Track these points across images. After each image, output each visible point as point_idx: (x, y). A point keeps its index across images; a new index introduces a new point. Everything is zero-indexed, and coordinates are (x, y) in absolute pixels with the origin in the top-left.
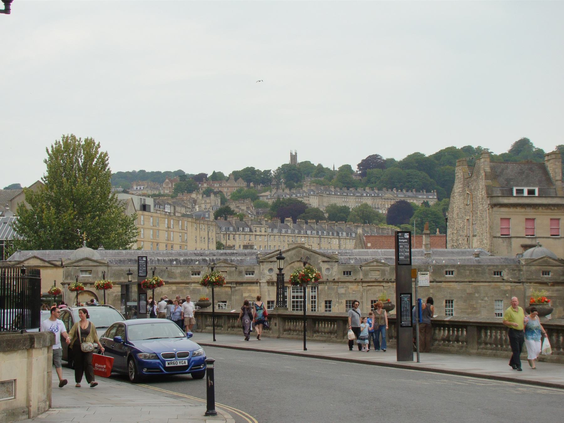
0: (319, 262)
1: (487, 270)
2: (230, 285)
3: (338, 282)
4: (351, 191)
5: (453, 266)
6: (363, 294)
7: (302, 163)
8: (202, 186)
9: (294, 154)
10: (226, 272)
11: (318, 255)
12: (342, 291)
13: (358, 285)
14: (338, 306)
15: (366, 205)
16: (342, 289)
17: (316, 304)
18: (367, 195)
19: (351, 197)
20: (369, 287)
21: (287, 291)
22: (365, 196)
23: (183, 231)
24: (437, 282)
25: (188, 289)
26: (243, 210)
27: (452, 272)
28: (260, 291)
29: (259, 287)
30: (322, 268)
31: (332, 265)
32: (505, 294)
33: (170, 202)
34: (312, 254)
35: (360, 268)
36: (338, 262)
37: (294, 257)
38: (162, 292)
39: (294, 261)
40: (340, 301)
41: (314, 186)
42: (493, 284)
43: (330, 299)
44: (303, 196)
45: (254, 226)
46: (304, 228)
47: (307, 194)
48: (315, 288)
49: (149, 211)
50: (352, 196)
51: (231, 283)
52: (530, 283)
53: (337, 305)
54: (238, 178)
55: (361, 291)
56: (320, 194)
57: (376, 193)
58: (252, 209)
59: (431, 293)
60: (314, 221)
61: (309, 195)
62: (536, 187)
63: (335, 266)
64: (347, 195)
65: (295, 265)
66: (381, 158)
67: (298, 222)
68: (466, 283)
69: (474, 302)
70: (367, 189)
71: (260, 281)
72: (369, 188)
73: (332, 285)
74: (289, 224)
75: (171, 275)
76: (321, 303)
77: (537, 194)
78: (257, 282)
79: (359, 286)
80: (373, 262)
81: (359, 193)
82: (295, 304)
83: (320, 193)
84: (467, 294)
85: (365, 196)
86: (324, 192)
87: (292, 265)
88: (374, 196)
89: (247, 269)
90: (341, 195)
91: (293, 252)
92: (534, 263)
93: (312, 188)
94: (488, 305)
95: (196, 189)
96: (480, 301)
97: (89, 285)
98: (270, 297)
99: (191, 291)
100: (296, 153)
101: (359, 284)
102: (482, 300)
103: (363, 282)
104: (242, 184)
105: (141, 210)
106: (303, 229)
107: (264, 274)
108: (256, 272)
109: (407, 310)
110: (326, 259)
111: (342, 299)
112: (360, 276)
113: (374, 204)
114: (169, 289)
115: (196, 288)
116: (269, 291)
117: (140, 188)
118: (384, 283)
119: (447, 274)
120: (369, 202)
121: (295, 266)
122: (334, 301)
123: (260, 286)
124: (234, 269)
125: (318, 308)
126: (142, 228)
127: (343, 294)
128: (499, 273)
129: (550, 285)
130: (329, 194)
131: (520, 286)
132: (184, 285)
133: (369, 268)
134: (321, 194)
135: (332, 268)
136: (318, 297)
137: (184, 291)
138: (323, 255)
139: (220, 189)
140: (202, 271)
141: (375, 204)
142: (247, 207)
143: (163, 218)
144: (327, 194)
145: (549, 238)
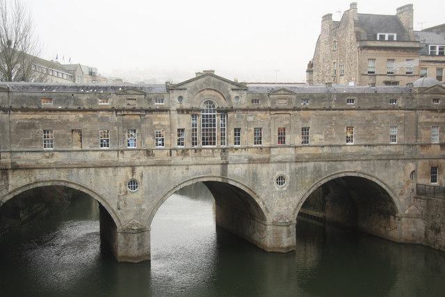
1: (384, 99)
2: (139, 113)
5: (354, 94)
12: (250, 119)
24: (339, 110)
27: (353, 100)
28: (170, 119)
52: (423, 110)
62: (394, 33)
75: (76, 101)
77: (395, 39)
78: (162, 110)
80: (280, 90)
96: (377, 128)
102: (380, 127)
103: (270, 110)
108: (166, 99)
109: (102, 156)
110: (234, 87)
112: (269, 105)
116: (179, 119)
124: (143, 96)
128: (392, 101)
131: (413, 113)
132: (92, 113)
137: (92, 118)
145: (385, 75)
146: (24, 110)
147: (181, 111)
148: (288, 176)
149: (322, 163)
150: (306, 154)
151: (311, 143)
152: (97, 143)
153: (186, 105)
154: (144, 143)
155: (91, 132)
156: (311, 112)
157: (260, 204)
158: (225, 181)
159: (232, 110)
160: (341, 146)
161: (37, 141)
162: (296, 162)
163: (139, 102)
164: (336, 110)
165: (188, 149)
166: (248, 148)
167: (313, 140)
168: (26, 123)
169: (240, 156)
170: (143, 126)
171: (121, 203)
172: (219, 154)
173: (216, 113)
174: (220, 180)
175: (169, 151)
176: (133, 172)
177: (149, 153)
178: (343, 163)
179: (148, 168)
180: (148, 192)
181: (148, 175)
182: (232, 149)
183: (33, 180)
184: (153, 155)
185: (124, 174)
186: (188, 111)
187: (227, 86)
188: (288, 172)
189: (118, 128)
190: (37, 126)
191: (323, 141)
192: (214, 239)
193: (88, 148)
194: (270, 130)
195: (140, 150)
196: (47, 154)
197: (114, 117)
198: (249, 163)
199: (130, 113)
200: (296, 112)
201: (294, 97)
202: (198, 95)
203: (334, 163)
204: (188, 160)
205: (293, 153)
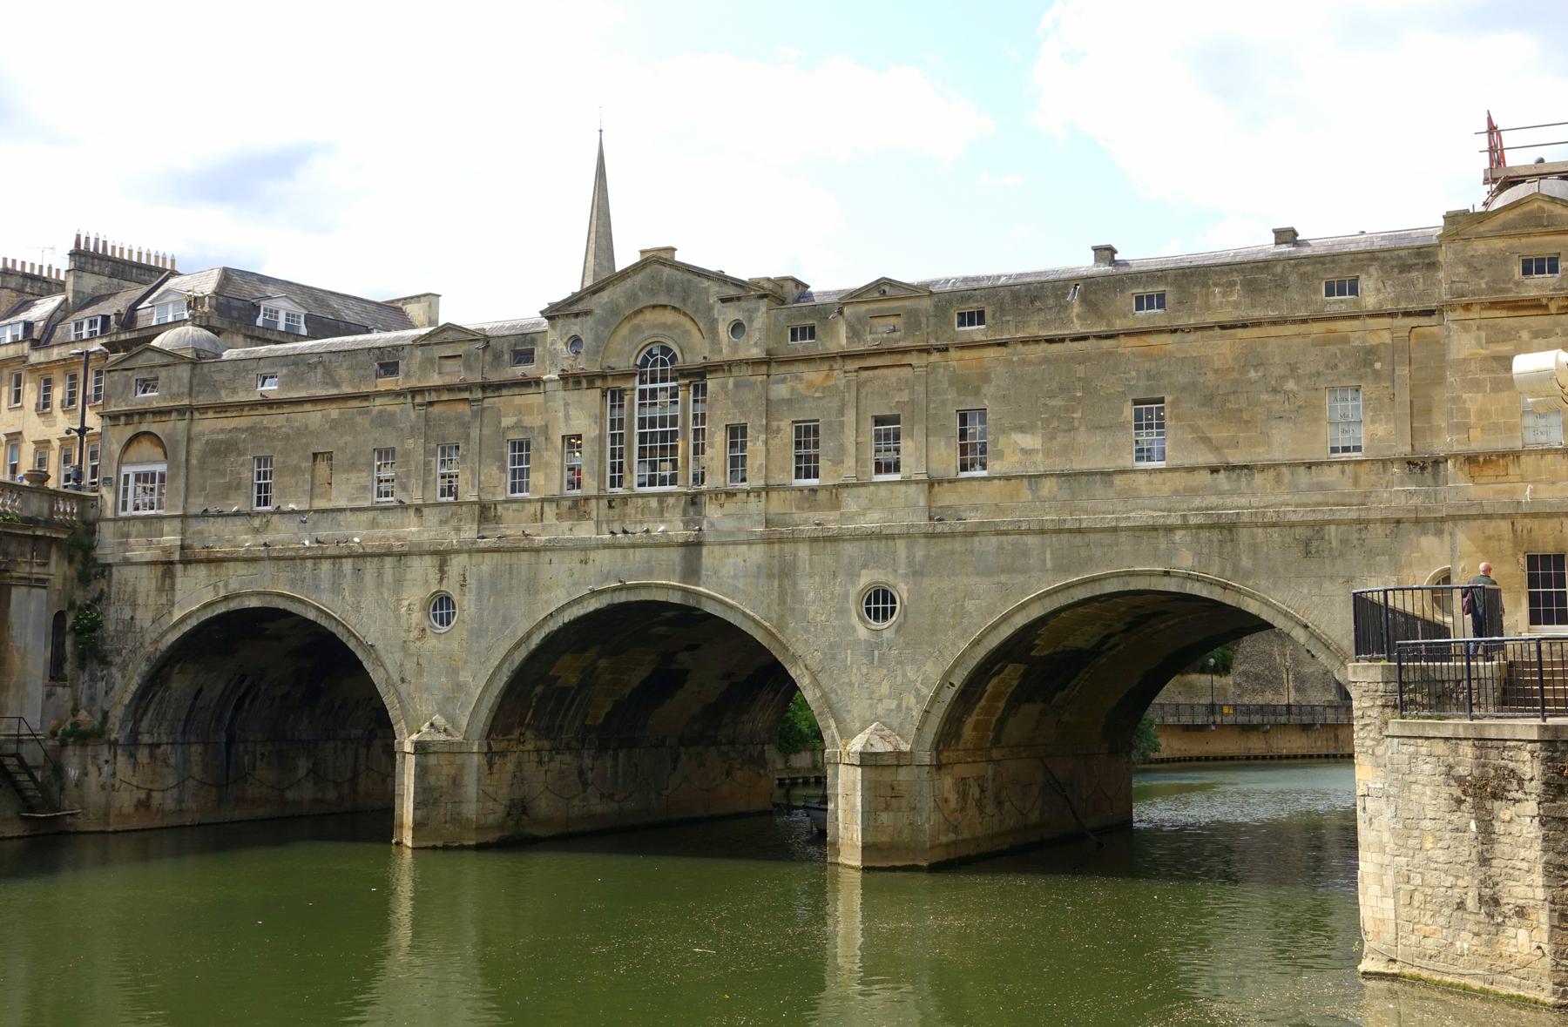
0: (711, 301)
2: (466, 395)
6: (847, 399)
10: (460, 356)
11: (706, 283)
12: (781, 391)
13: (831, 369)
17: (609, 461)
20: (865, 374)
25: (367, 413)
27: (1161, 297)
32: (1368, 363)
34: (689, 281)
37: (640, 294)
38: (306, 427)
39: (640, 305)
42: (1317, 329)
51: (469, 388)
52: (1467, 307)
59: (1080, 379)
63: (757, 310)
65: (644, 321)
68: (1211, 333)
69: (1243, 403)
73: (747, 372)
76: (715, 433)
84: (1216, 371)
87: (637, 320)
89: (515, 345)
91: (639, 278)
92: (1482, 229)
94: (1300, 407)
96: (1265, 397)
97: (149, 417)
98: (571, 423)
99: (372, 421)
101: (836, 366)
102: (1275, 391)
111: (781, 420)
114: (323, 416)
115: (385, 409)
116: (566, 405)
118: (915, 353)
119: (1140, 307)
121: (644, 325)
122: (754, 423)
129: (1554, 311)
132: (356, 403)
133: (865, 307)
135: (751, 320)
137: (359, 419)
138: (721, 278)
140: (403, 359)
146: (223, 408)
147: (571, 380)
149: (1031, 540)
151: (996, 467)
152: (365, 488)
153: (583, 365)
155: (352, 457)
156: (991, 353)
158: (692, 602)
159: (716, 368)
160: (1109, 474)
161: (238, 487)
163: (469, 367)
164: (1084, 338)
165: (587, 499)
168: (221, 442)
170: (475, 433)
171: (410, 665)
172: (679, 510)
175: (538, 505)
176: (442, 571)
177: (485, 512)
179: (477, 558)
180: (477, 633)
181: (480, 581)
182: (715, 494)
183: (222, 593)
184: (498, 519)
185: (421, 570)
186: (591, 379)
187: (706, 290)
190: (241, 446)
191: (1039, 458)
193: (343, 503)
194: (842, 425)
196: (257, 522)
197: (407, 413)
199: (445, 397)
200: (935, 357)
201: (926, 304)
202: (624, 331)
204: (585, 531)
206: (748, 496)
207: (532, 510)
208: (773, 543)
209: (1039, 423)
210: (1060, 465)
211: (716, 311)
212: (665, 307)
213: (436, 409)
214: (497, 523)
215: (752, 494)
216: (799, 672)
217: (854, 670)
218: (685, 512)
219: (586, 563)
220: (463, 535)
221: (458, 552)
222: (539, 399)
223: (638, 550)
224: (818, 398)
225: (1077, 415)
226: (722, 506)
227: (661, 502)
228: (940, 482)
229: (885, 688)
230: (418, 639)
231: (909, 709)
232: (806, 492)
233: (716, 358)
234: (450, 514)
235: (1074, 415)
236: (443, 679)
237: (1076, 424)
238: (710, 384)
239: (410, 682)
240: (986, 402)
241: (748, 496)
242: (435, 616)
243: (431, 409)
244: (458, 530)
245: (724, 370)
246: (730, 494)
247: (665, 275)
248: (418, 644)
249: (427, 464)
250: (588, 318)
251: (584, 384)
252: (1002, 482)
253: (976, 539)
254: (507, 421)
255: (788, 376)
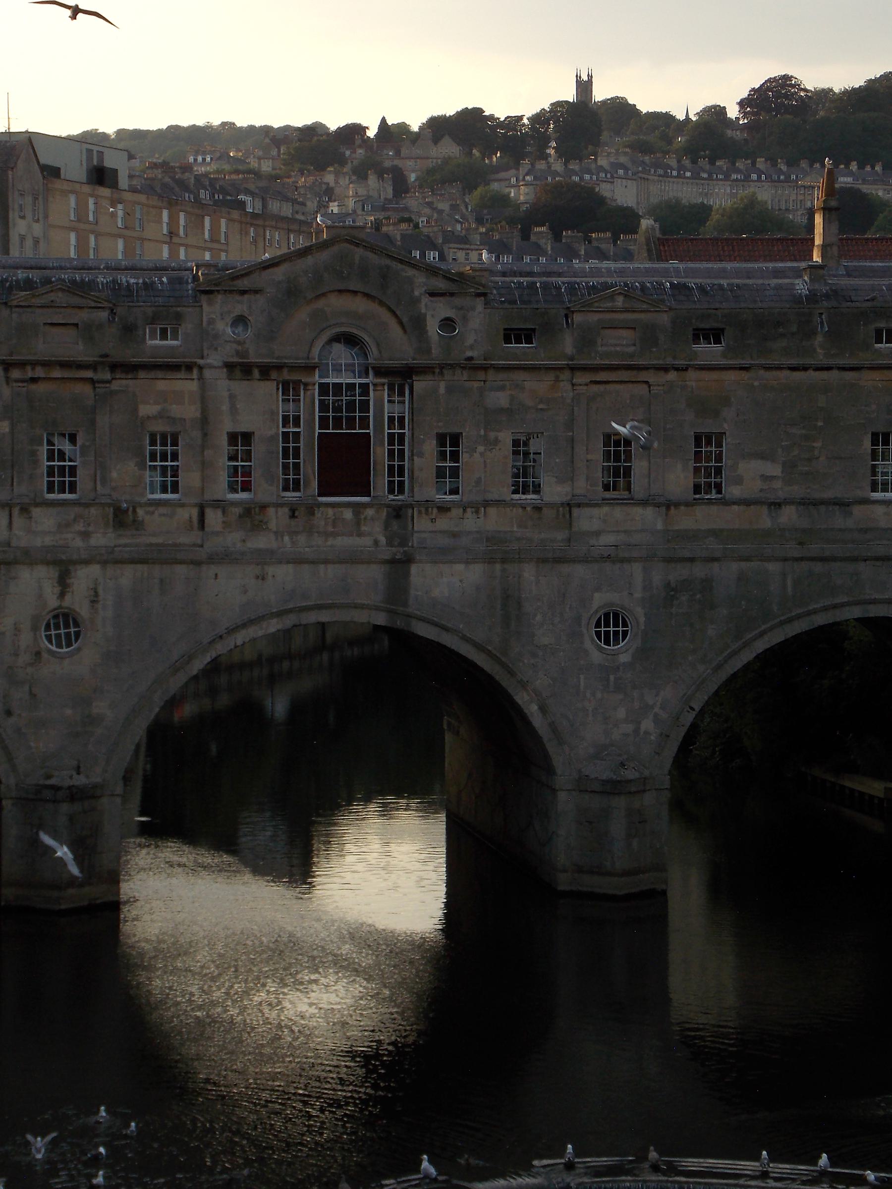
0: (417, 293)
2: (89, 374)
3: (485, 368)
4: (720, 168)
7: (604, 102)
8: (354, 155)
9: (585, 78)
10: (76, 325)
11: (410, 272)
14: (482, 454)
15: (752, 202)
16: (500, 394)
18: (759, 177)
19: (718, 182)
20: (595, 388)
21: (302, 398)
22: (755, 181)
23: (215, 246)
26: (440, 212)
29: (195, 383)
30: (428, 318)
31: (461, 308)
33: (252, 187)
35: (566, 316)
36: (484, 295)
40: (492, 435)
41: (625, 154)
43: (456, 430)
44: (597, 179)
45: (452, 245)
46: (583, 252)
47: (609, 176)
48: (402, 393)
49: (114, 185)
50: (721, 180)
53: (481, 449)
54: (442, 136)
55: (569, 401)
56: (640, 175)
57: (783, 173)
58: (464, 210)
60: (609, 234)
61: (612, 177)
64: (710, 178)
66: (797, 85)
67: (566, 237)
70: (761, 163)
71: (201, 362)
72: (766, 160)
73: (461, 377)
74: (542, 242)
79: (562, 384)
81: (738, 171)
82: (396, 447)
83: (640, 172)
85: (755, 181)
86: (652, 171)
87: (321, 304)
88: (779, 181)
90: (696, 179)
93: (622, 159)
95: (341, 161)
100: (590, 77)
101: (562, 377)
104: (449, 149)
105: (90, 182)
106: (580, 255)
107: (216, 336)
110: (440, 284)
111: (499, 431)
113: (777, 200)
116: (232, 397)
117: (204, 160)
118: (652, 371)
120: (765, 194)
122: (469, 432)
123: (201, 378)
125: (411, 459)
126: (93, 232)
127: (501, 410)
130: (666, 175)
133: (595, 317)
134: (643, 176)
135: (465, 319)
136: (412, 420)
139: (397, 162)
141: (779, 201)
142: (451, 205)
143: (154, 207)
144: (660, 176)
148: (639, 612)
149: (773, 567)
150: (715, 533)
151: (733, 491)
154: (104, 481)
157: (532, 710)
158: (399, 624)
160: (848, 505)
162: (669, 560)
164: (829, 369)
165: (263, 507)
166: (487, 504)
167: (739, 481)
169: (455, 535)
170: (103, 421)
171: (852, 254)
173: (370, 379)
174: (381, 619)
175: (195, 512)
176: (63, 583)
178: (565, 569)
182: (427, 504)
184: (138, 525)
188: (638, 595)
189: (13, 426)
191: (778, 484)
192: (415, 632)
195: (87, 505)
198: (491, 561)
199: (160, 377)
200: (672, 376)
202: (303, 314)
203: (818, 567)
204: (262, 542)
205: (660, 526)
206: (465, 511)
207: (187, 516)
208: (495, 562)
209: (780, 450)
210: (797, 491)
211: (423, 305)
212: (355, 293)
213: (41, 388)
214: (137, 529)
215: (469, 510)
216: (526, 698)
217: (588, 695)
218: (387, 526)
219: (263, 579)
220: (93, 542)
221: (87, 562)
222: (192, 386)
223: (330, 567)
224: (541, 409)
225: (818, 444)
226: (433, 521)
227: (356, 514)
228: (677, 505)
229: (621, 713)
230: (31, 665)
231: (647, 733)
232: (529, 509)
233: (422, 361)
234: (72, 517)
235: (815, 445)
236: (69, 712)
237: (816, 453)
238: (417, 386)
239: (20, 715)
240: (725, 426)
241: (465, 511)
242: (598, 634)
243: (33, 387)
244: (85, 535)
245: (434, 373)
246: (444, 509)
247: (357, 258)
248: (30, 670)
249: (34, 453)
250: (258, 296)
251: (256, 373)
252: (742, 508)
253: (716, 565)
254: (146, 410)
255: (507, 383)
